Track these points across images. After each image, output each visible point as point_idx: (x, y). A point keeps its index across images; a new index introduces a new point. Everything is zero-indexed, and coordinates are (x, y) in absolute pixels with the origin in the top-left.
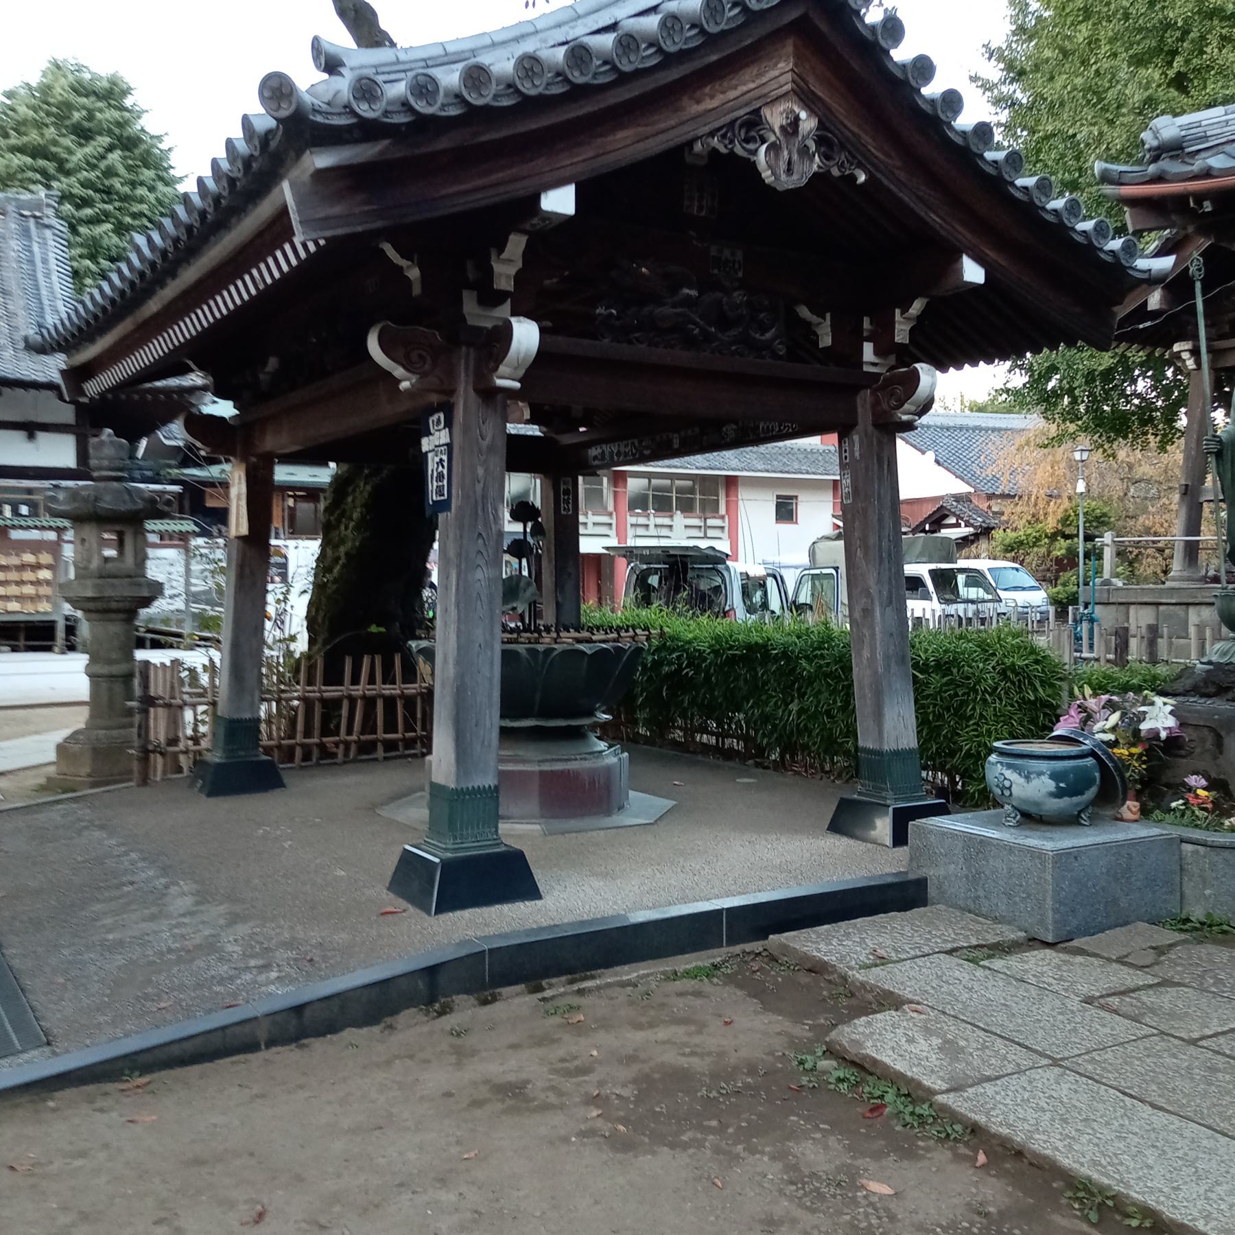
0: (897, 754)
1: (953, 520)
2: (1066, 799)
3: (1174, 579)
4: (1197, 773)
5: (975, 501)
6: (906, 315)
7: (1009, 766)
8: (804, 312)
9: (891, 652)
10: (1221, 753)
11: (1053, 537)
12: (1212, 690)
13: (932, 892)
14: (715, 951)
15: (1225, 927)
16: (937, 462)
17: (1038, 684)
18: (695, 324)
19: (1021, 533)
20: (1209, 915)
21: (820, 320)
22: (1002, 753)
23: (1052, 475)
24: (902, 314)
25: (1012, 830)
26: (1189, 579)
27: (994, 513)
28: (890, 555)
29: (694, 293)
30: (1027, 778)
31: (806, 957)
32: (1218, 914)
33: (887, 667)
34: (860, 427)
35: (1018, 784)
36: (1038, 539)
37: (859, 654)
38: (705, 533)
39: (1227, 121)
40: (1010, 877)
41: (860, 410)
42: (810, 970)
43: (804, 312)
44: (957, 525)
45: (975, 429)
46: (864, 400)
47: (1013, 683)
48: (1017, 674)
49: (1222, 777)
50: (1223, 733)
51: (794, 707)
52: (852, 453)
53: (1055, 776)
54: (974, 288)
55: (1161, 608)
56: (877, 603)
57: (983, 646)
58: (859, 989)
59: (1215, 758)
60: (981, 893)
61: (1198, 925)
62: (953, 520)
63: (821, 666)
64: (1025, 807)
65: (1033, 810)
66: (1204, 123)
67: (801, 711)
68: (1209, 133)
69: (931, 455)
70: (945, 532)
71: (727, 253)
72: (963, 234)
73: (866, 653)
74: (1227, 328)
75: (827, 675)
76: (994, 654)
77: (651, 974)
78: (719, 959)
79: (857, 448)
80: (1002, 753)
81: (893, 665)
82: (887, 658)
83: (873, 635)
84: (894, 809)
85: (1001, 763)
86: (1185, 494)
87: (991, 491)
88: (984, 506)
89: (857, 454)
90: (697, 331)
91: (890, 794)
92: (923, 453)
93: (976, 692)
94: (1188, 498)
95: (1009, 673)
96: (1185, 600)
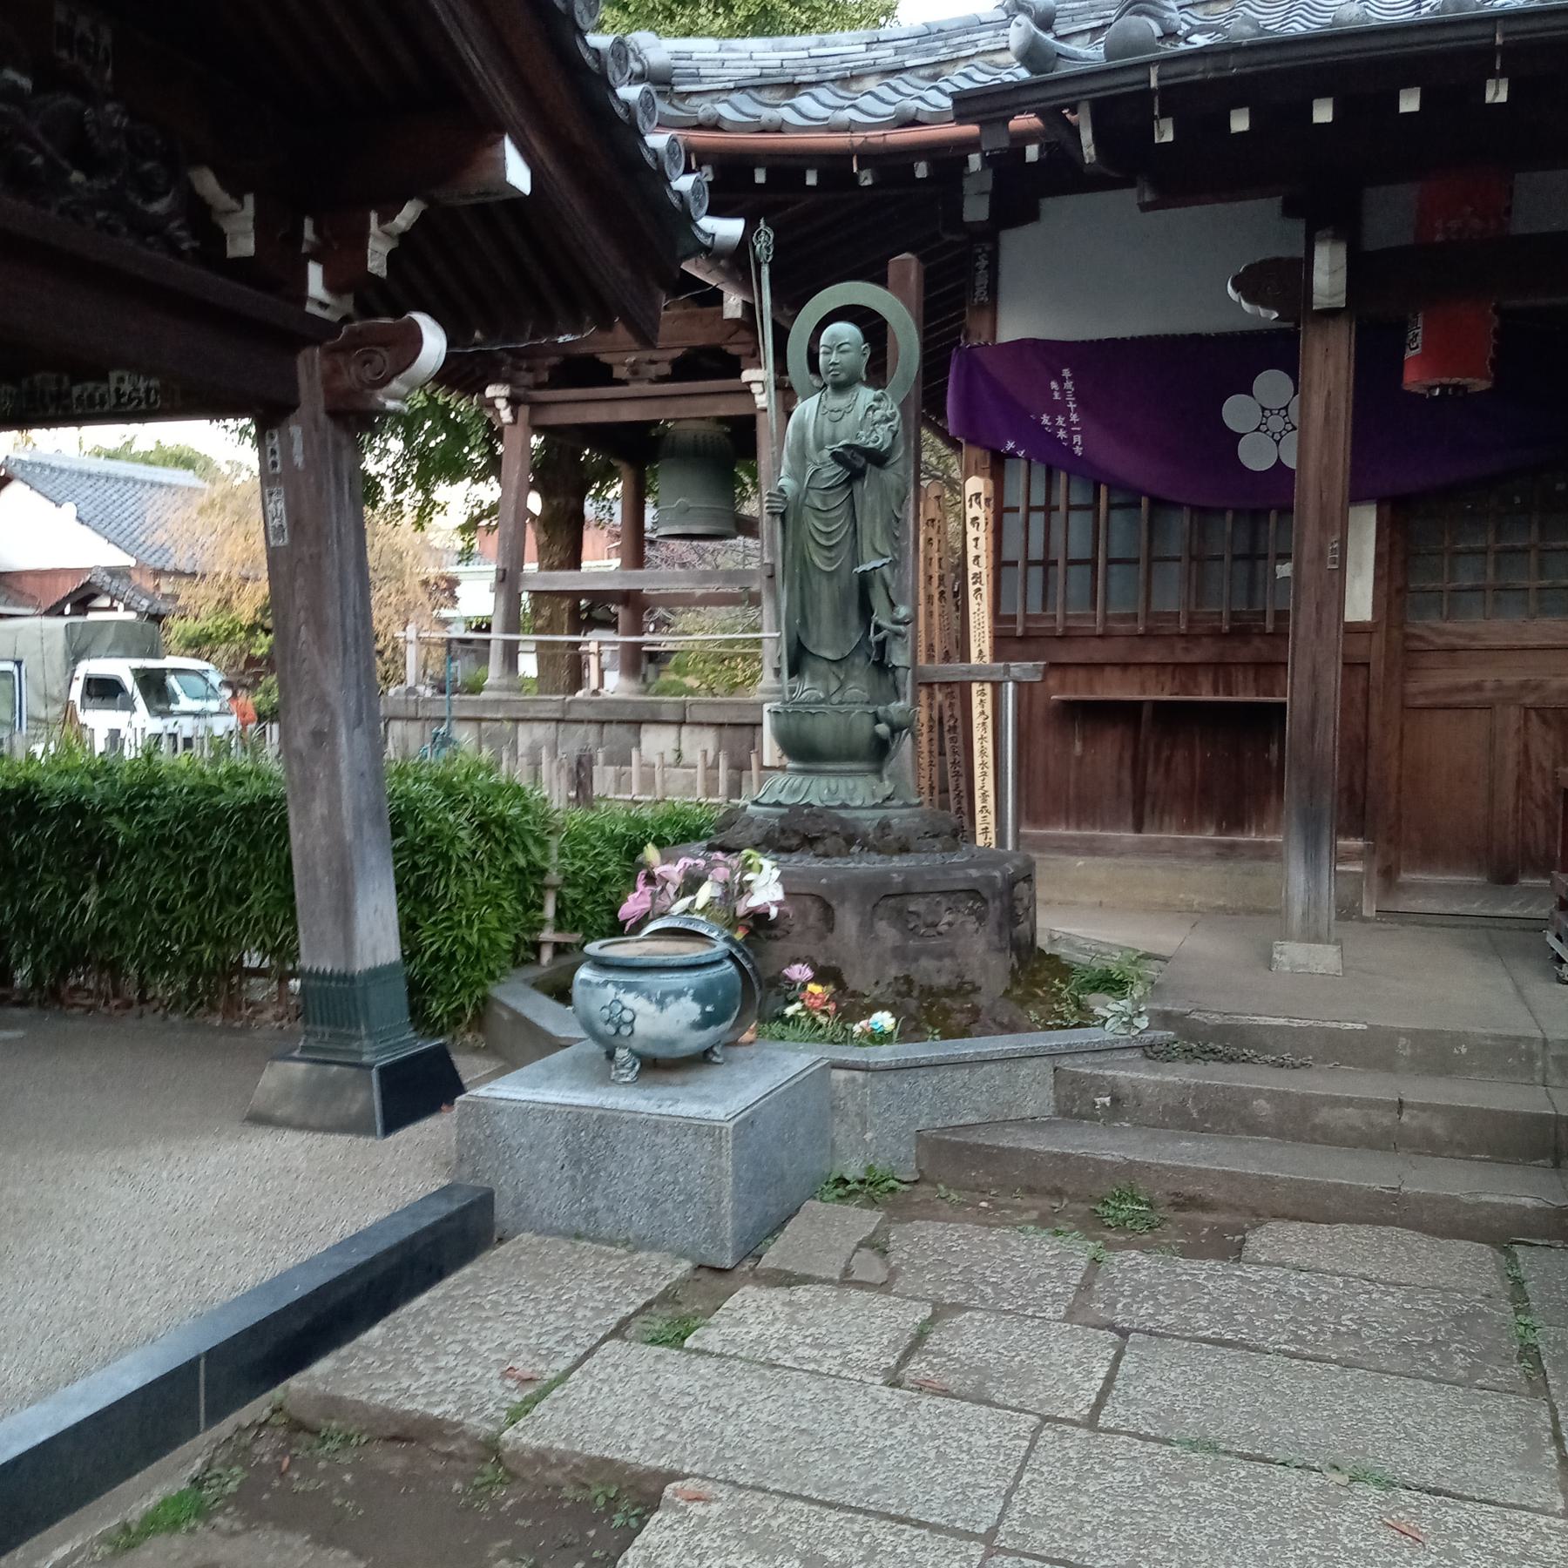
0: (376, 974)
1: (104, 602)
2: (712, 1029)
3: (491, 688)
4: (797, 961)
5: (136, 577)
6: (388, 226)
7: (629, 987)
8: (207, 183)
9: (363, 805)
10: (831, 930)
11: (252, 630)
12: (795, 841)
13: (503, 1212)
14: (186, 1449)
15: (892, 1183)
16: (79, 519)
17: (530, 842)
18: (33, 143)
19: (210, 623)
20: (870, 1169)
21: (234, 204)
22: (602, 964)
23: (246, 549)
24: (381, 222)
25: (630, 1088)
26: (509, 688)
27: (164, 596)
28: (357, 640)
29: (26, 83)
30: (661, 1003)
31: (387, 1414)
32: (881, 1165)
33: (358, 830)
34: (303, 411)
35: (645, 1016)
36: (231, 633)
37: (305, 808)
38: (1038, 509)
39: (723, 61)
40: (658, 1170)
41: (303, 380)
42: (395, 1438)
43: (207, 183)
44: (112, 608)
45: (127, 480)
46: (310, 367)
47: (498, 842)
48: (504, 829)
49: (833, 963)
50: (834, 903)
51: (91, 898)
52: (288, 457)
53: (700, 997)
54: (515, 201)
55: (484, 725)
56: (341, 721)
57: (447, 787)
58: (530, 1464)
59: (822, 938)
60: (599, 1203)
61: (856, 1186)
62: (105, 602)
63: (147, 827)
64: (651, 1050)
65: (661, 1052)
66: (696, 56)
67: (106, 905)
68: (702, 72)
69: (69, 509)
70: (92, 616)
71: (83, 25)
72: (508, 104)
73: (319, 808)
74: (545, 377)
75: (163, 841)
76: (465, 800)
77: (81, 1550)
78: (199, 1462)
79: (298, 447)
80: (602, 964)
81: (366, 825)
82: (358, 815)
83: (334, 776)
84: (383, 1071)
85: (616, 984)
86: (503, 580)
87: (159, 565)
88: (149, 585)
89: (299, 460)
90: (38, 160)
91: (367, 1045)
92: (58, 505)
93: (449, 860)
94: (506, 585)
95: (493, 828)
96: (514, 715)
